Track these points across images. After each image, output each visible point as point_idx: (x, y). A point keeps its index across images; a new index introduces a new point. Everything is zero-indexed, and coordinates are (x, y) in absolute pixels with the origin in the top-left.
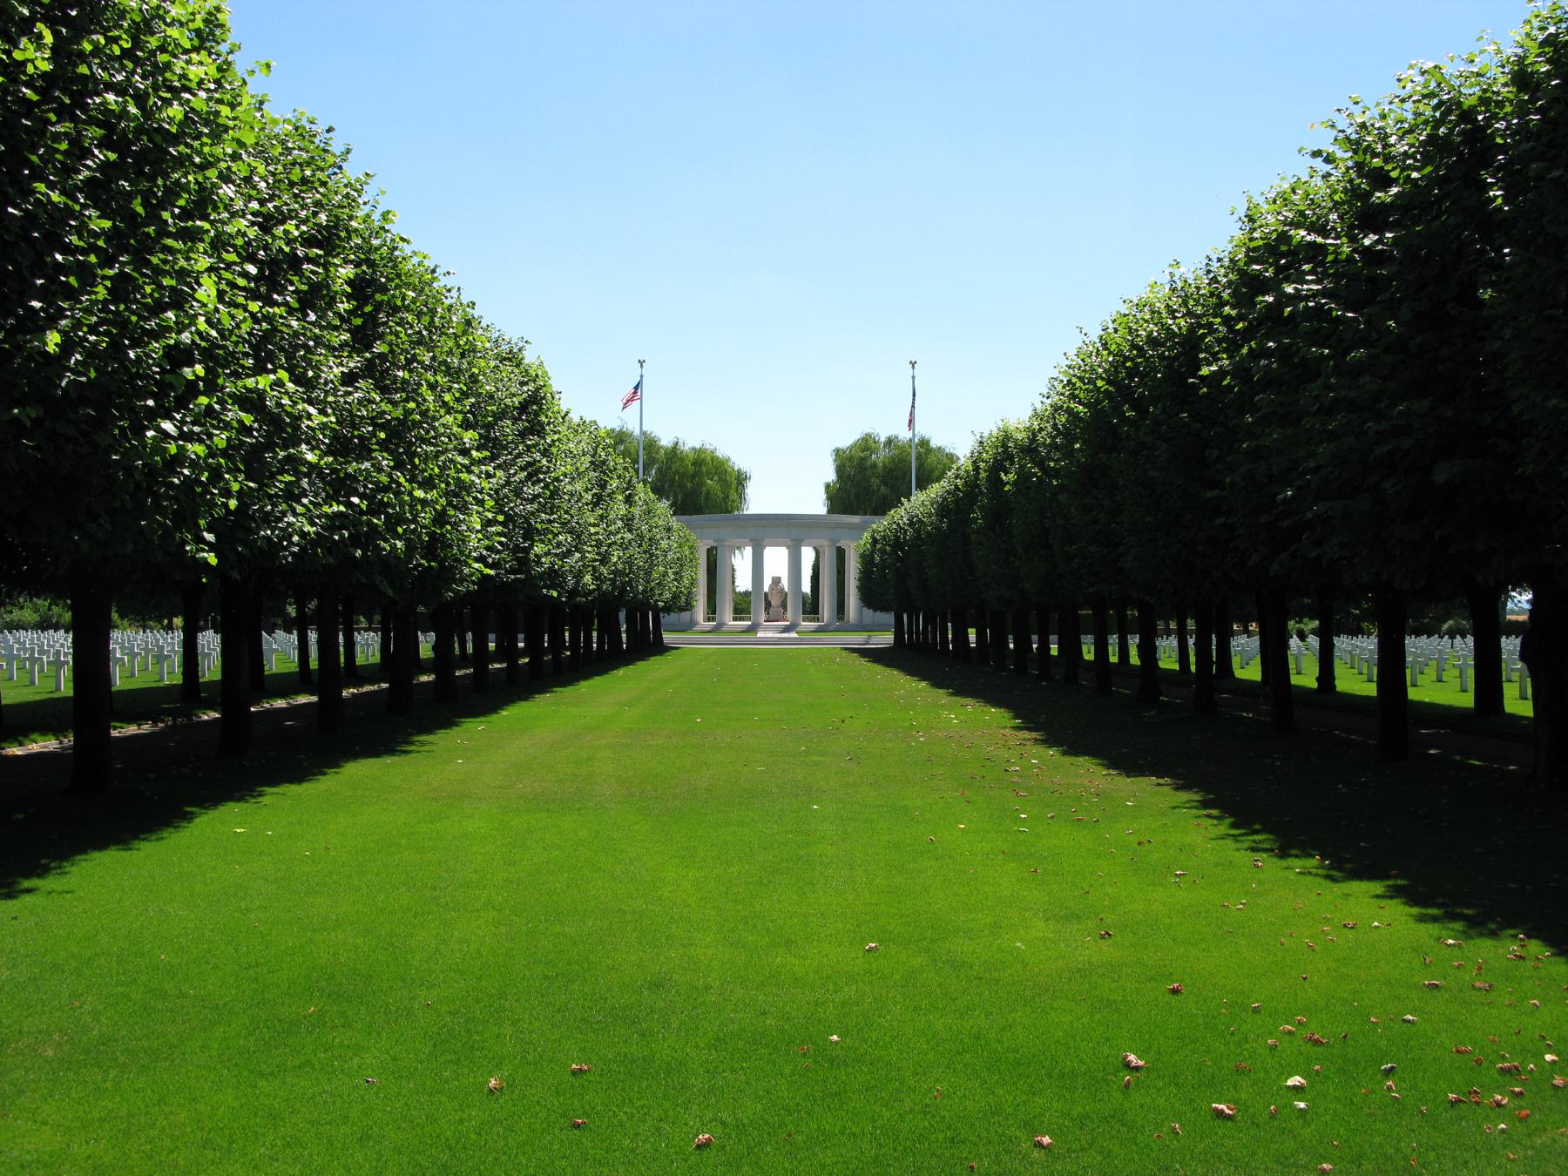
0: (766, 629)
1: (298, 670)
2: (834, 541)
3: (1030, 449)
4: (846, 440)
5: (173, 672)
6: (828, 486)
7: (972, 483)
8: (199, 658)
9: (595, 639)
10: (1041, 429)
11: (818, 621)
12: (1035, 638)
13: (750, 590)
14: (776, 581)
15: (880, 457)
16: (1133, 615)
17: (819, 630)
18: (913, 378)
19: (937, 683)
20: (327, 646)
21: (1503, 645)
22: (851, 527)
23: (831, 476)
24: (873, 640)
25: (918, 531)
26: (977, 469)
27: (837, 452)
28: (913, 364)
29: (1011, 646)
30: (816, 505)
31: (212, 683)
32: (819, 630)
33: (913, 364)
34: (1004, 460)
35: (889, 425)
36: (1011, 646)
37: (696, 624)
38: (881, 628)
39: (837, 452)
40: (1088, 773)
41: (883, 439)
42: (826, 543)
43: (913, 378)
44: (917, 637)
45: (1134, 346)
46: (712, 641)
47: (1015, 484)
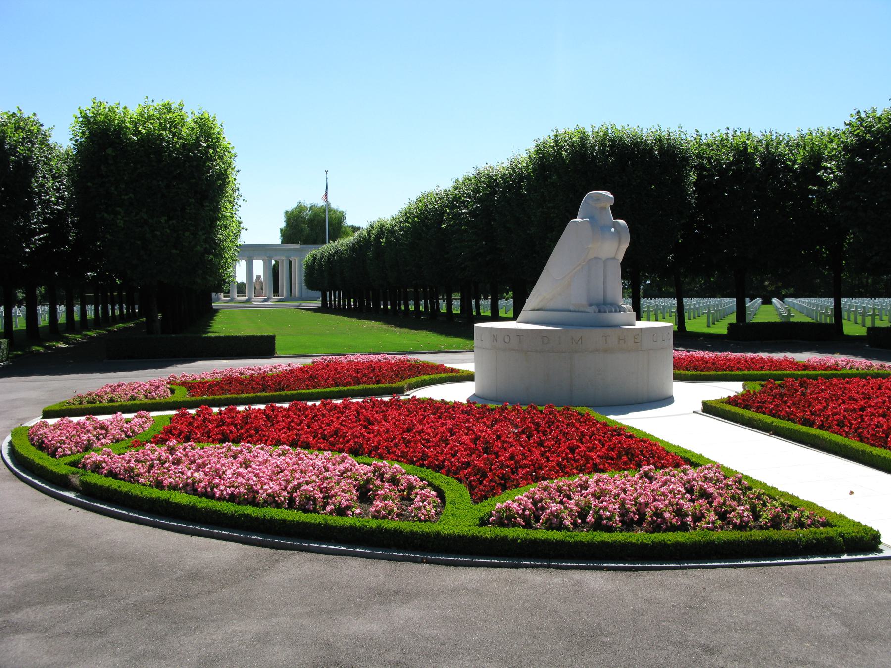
0: (255, 301)
1: (66, 322)
2: (288, 258)
3: (391, 231)
4: (291, 206)
5: (45, 320)
6: (282, 230)
7: (367, 241)
8: (13, 318)
9: (352, 304)
10: (395, 225)
11: (278, 296)
12: (382, 302)
13: (245, 281)
14: (259, 277)
15: (308, 214)
16: (790, 176)
17: (279, 301)
18: (327, 178)
19: (360, 318)
20: (105, 310)
21: (642, 302)
22: (296, 250)
23: (283, 225)
24: (303, 305)
25: (340, 257)
26: (370, 236)
27: (286, 212)
28: (326, 172)
29: (382, 306)
30: (275, 239)
31: (44, 327)
32: (279, 301)
33: (326, 172)
34: (380, 234)
35: (313, 199)
36: (382, 306)
37: (220, 299)
38: (315, 299)
39: (286, 212)
40: (412, 331)
41: (309, 206)
42: (283, 258)
43: (327, 178)
44: (335, 303)
45: (426, 211)
46: (288, 306)
47: (385, 243)
